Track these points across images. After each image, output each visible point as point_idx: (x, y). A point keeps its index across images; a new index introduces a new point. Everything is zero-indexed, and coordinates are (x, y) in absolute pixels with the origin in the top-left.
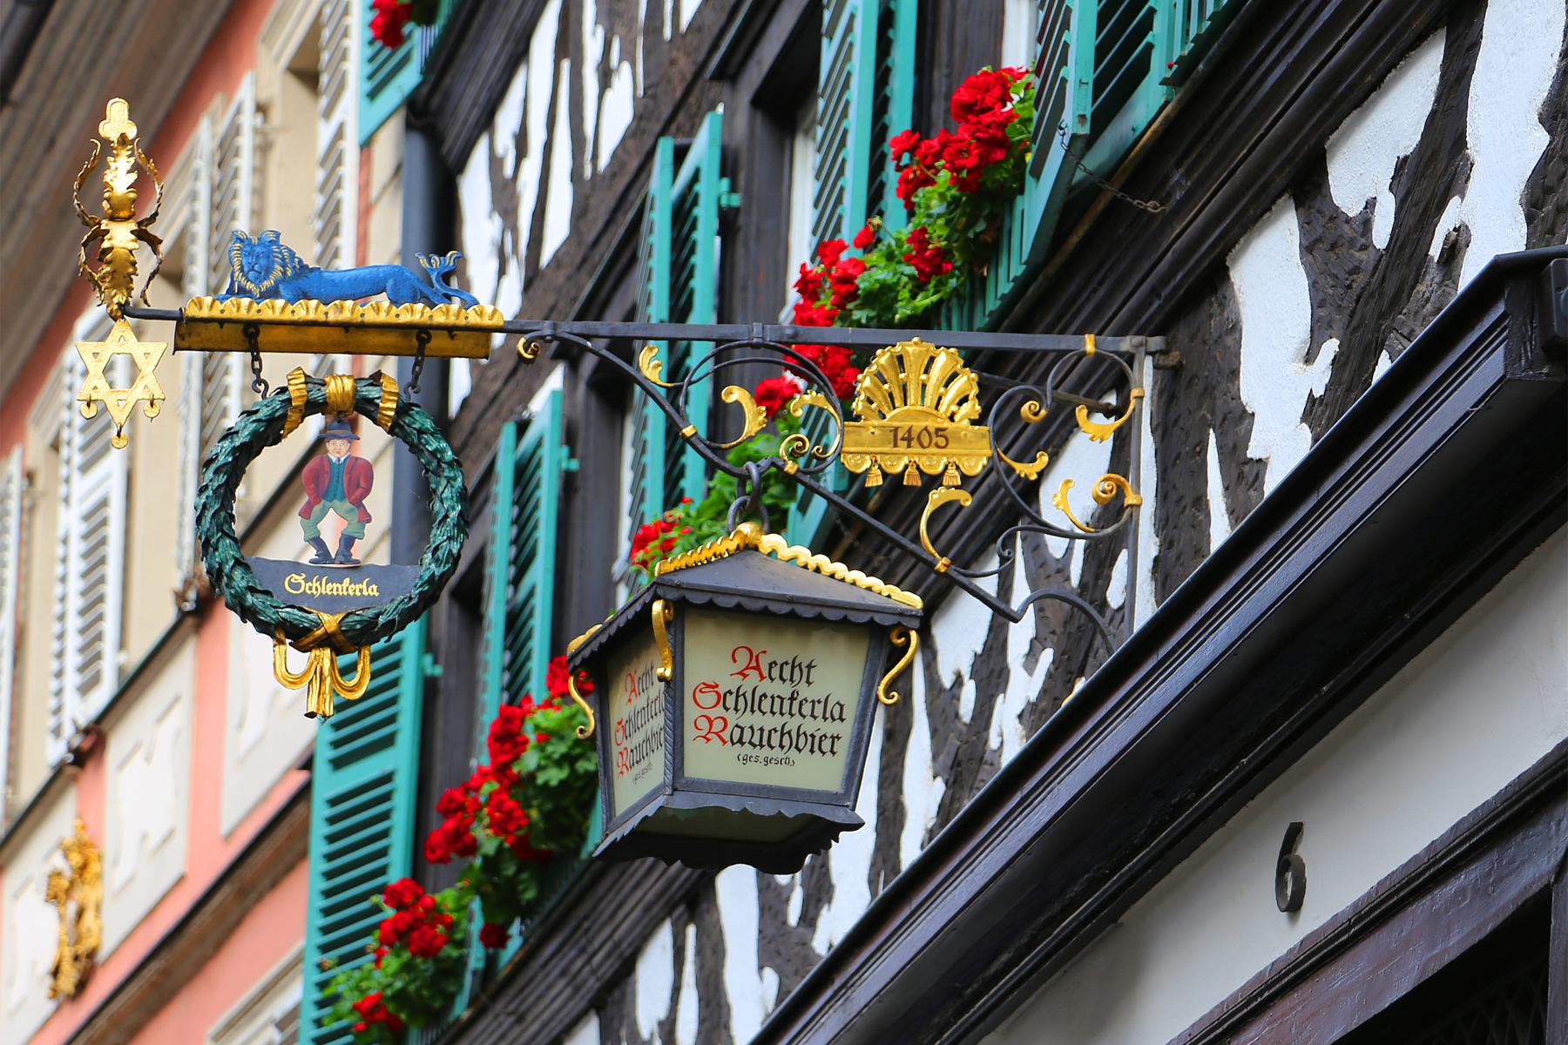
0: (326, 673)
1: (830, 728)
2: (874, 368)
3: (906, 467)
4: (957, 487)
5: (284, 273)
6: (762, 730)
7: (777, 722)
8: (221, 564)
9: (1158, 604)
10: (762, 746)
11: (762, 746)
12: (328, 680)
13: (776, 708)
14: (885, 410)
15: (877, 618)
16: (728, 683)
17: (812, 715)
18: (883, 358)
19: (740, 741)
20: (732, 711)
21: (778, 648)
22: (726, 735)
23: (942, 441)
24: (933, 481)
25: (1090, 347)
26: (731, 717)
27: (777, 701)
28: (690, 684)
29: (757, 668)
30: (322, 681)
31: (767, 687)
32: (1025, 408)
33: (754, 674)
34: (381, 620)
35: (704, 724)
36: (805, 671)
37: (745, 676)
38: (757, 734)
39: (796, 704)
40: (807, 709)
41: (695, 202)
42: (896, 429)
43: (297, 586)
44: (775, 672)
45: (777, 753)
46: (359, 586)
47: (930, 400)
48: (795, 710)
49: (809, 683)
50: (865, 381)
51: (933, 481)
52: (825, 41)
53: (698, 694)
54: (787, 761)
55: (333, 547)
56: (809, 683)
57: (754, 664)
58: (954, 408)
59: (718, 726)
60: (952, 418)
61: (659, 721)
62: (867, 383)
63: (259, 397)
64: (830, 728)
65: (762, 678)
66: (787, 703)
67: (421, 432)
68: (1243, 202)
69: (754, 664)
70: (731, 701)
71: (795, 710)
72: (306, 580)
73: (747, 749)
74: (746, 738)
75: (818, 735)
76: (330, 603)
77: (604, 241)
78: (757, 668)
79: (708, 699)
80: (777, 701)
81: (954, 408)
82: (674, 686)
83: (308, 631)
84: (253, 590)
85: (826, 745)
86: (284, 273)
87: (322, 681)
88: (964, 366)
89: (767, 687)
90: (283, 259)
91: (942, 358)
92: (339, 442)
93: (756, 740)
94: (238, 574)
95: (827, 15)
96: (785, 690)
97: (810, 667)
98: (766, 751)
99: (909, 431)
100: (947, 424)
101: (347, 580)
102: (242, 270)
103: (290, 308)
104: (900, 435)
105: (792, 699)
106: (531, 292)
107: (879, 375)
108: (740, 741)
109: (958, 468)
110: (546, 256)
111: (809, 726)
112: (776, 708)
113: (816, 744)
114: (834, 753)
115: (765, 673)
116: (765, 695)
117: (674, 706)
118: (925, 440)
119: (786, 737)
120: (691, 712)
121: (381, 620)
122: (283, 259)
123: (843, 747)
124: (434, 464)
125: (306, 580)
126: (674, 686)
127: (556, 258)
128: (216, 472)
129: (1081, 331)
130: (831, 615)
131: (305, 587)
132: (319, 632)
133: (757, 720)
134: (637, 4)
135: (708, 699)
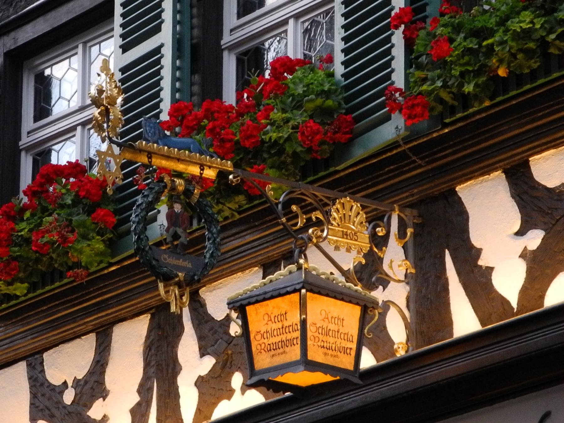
29: (271, 320)
33: (270, 322)
43: (165, 259)
45: (281, 350)
54: (284, 352)
66: (281, 330)
73: (273, 352)
84: (154, 259)
85: (348, 351)
125: (169, 257)
132: (177, 279)
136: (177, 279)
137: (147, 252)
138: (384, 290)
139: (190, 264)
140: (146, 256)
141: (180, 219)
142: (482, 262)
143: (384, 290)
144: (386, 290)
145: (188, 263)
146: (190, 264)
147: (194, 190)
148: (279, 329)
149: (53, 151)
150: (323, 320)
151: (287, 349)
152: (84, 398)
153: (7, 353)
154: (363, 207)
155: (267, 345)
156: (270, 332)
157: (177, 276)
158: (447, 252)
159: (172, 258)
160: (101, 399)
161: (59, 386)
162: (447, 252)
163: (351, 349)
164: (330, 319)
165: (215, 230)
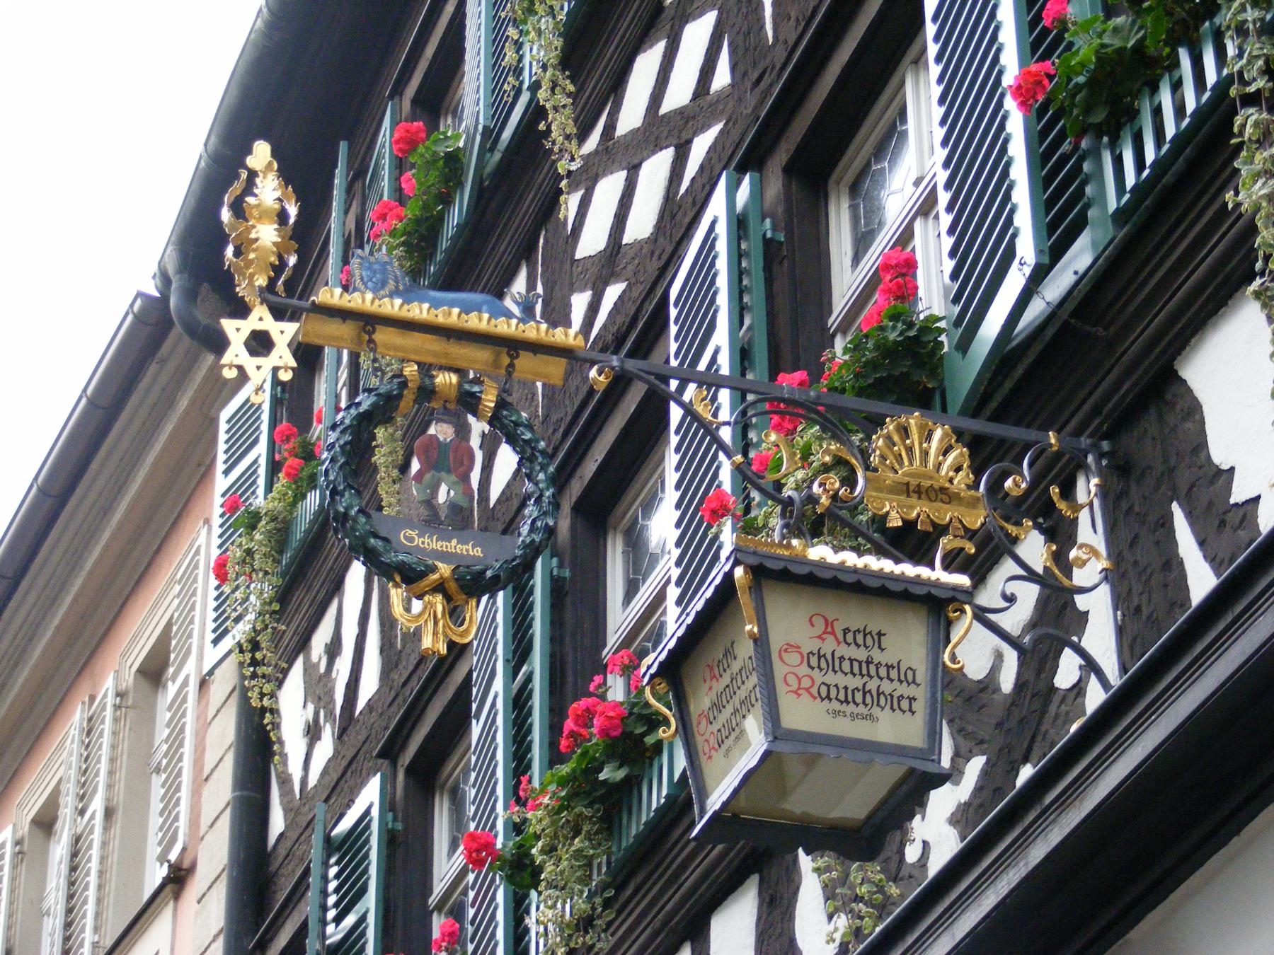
0: (439, 615)
1: (904, 690)
3: (919, 515)
4: (962, 537)
5: (397, 287)
6: (846, 688)
7: (856, 682)
8: (346, 508)
10: (848, 703)
11: (848, 703)
12: (441, 623)
13: (856, 670)
14: (897, 467)
15: (934, 591)
17: (888, 677)
18: (891, 426)
19: (828, 696)
20: (817, 670)
21: (853, 615)
22: (814, 691)
24: (942, 530)
25: (1052, 438)
28: (776, 642)
29: (833, 633)
30: (436, 623)
31: (843, 651)
32: (1009, 483)
33: (830, 638)
34: (489, 573)
36: (876, 638)
37: (823, 640)
38: (842, 692)
41: (306, 936)
42: (908, 484)
43: (411, 540)
44: (850, 637)
45: (861, 709)
46: (465, 547)
47: (931, 465)
51: (942, 530)
52: (474, 721)
53: (783, 654)
57: (829, 629)
58: (951, 474)
60: (951, 481)
61: (754, 679)
62: (881, 442)
63: (377, 381)
64: (904, 690)
65: (839, 643)
66: (864, 665)
67: (517, 424)
68: (1110, 405)
70: (814, 661)
71: (873, 672)
73: (835, 705)
74: (833, 695)
76: (445, 557)
77: (415, 678)
78: (833, 633)
79: (793, 658)
81: (951, 474)
82: (761, 642)
83: (423, 575)
84: (376, 536)
85: (905, 704)
86: (397, 287)
87: (436, 623)
88: (957, 441)
89: (843, 651)
90: (396, 277)
91: (938, 433)
92: (445, 425)
93: (842, 697)
94: (363, 519)
95: (474, 706)
96: (861, 654)
97: (880, 634)
100: (947, 485)
102: (362, 279)
103: (406, 307)
104: (911, 488)
106: (345, 738)
107: (888, 438)
108: (828, 696)
109: (961, 522)
110: (361, 704)
111: (887, 687)
113: (895, 703)
114: (913, 713)
117: (764, 663)
119: (868, 695)
120: (779, 670)
121: (489, 573)
122: (396, 277)
124: (529, 451)
126: (761, 642)
127: (370, 705)
128: (343, 432)
129: (1045, 428)
130: (893, 587)
131: (418, 541)
132: (436, 576)
134: (760, 6)
135: (793, 658)
136: (436, 576)
137: (355, 520)
140: (353, 529)
141: (451, 455)
142: (1238, 495)
147: (520, 416)
149: (1067, 652)
150: (819, 637)
154: (959, 434)
157: (434, 569)
158: (1175, 507)
159: (431, 537)
161: (286, 827)
162: (1175, 507)
163: (912, 699)
164: (840, 636)
165: (541, 476)
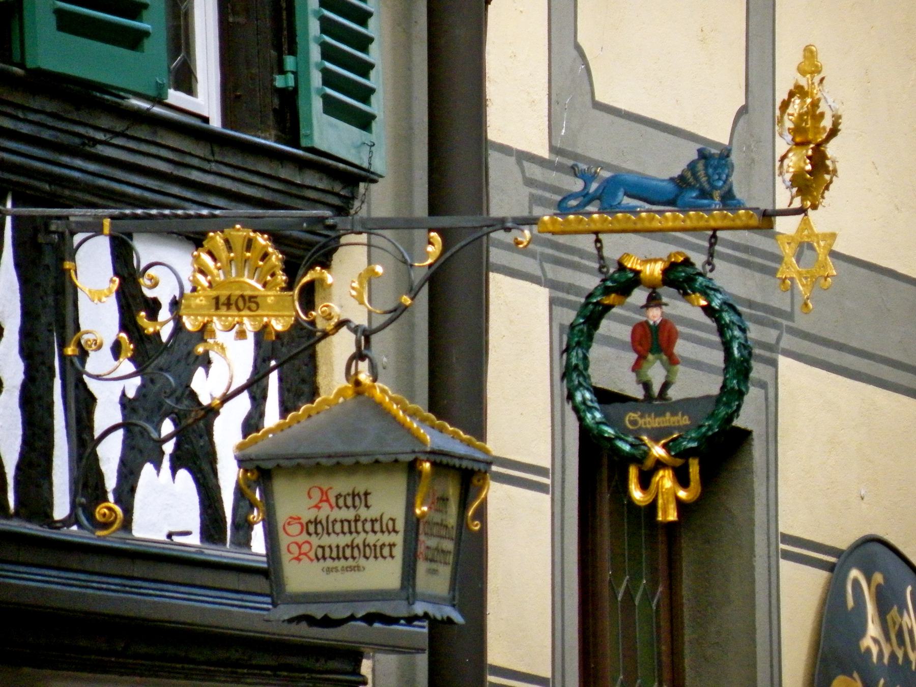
1: (386, 538)
2: (270, 250)
9: (245, 436)
16: (308, 515)
19: (324, 558)
23: (253, 306)
26: (315, 540)
27: (346, 524)
29: (327, 501)
33: (325, 505)
35: (294, 549)
36: (363, 498)
38: (335, 550)
39: (360, 524)
40: (368, 526)
43: (634, 422)
45: (351, 562)
48: (360, 528)
49: (367, 506)
50: (276, 258)
53: (287, 528)
54: (357, 568)
55: (656, 389)
56: (367, 506)
59: (305, 548)
64: (386, 538)
66: (353, 524)
69: (324, 498)
70: (312, 528)
71: (360, 528)
72: (642, 417)
73: (329, 563)
74: (327, 554)
75: (379, 544)
78: (327, 501)
79: (295, 529)
80: (346, 524)
85: (386, 551)
93: (334, 555)
96: (350, 514)
97: (366, 494)
98: (342, 563)
99: (229, 298)
101: (668, 414)
105: (356, 521)
111: (371, 539)
112: (346, 529)
113: (378, 552)
115: (334, 504)
116: (366, 520)
118: (241, 304)
123: (398, 551)
125: (642, 417)
133: (333, 540)
138: (207, 373)
139: (686, 417)
143: (207, 373)
144: (119, 394)
145: (683, 415)
146: (686, 417)
148: (349, 522)
151: (362, 562)
152: (272, 52)
153: (64, 584)
155: (314, 547)
156: (324, 522)
160: (200, 371)
